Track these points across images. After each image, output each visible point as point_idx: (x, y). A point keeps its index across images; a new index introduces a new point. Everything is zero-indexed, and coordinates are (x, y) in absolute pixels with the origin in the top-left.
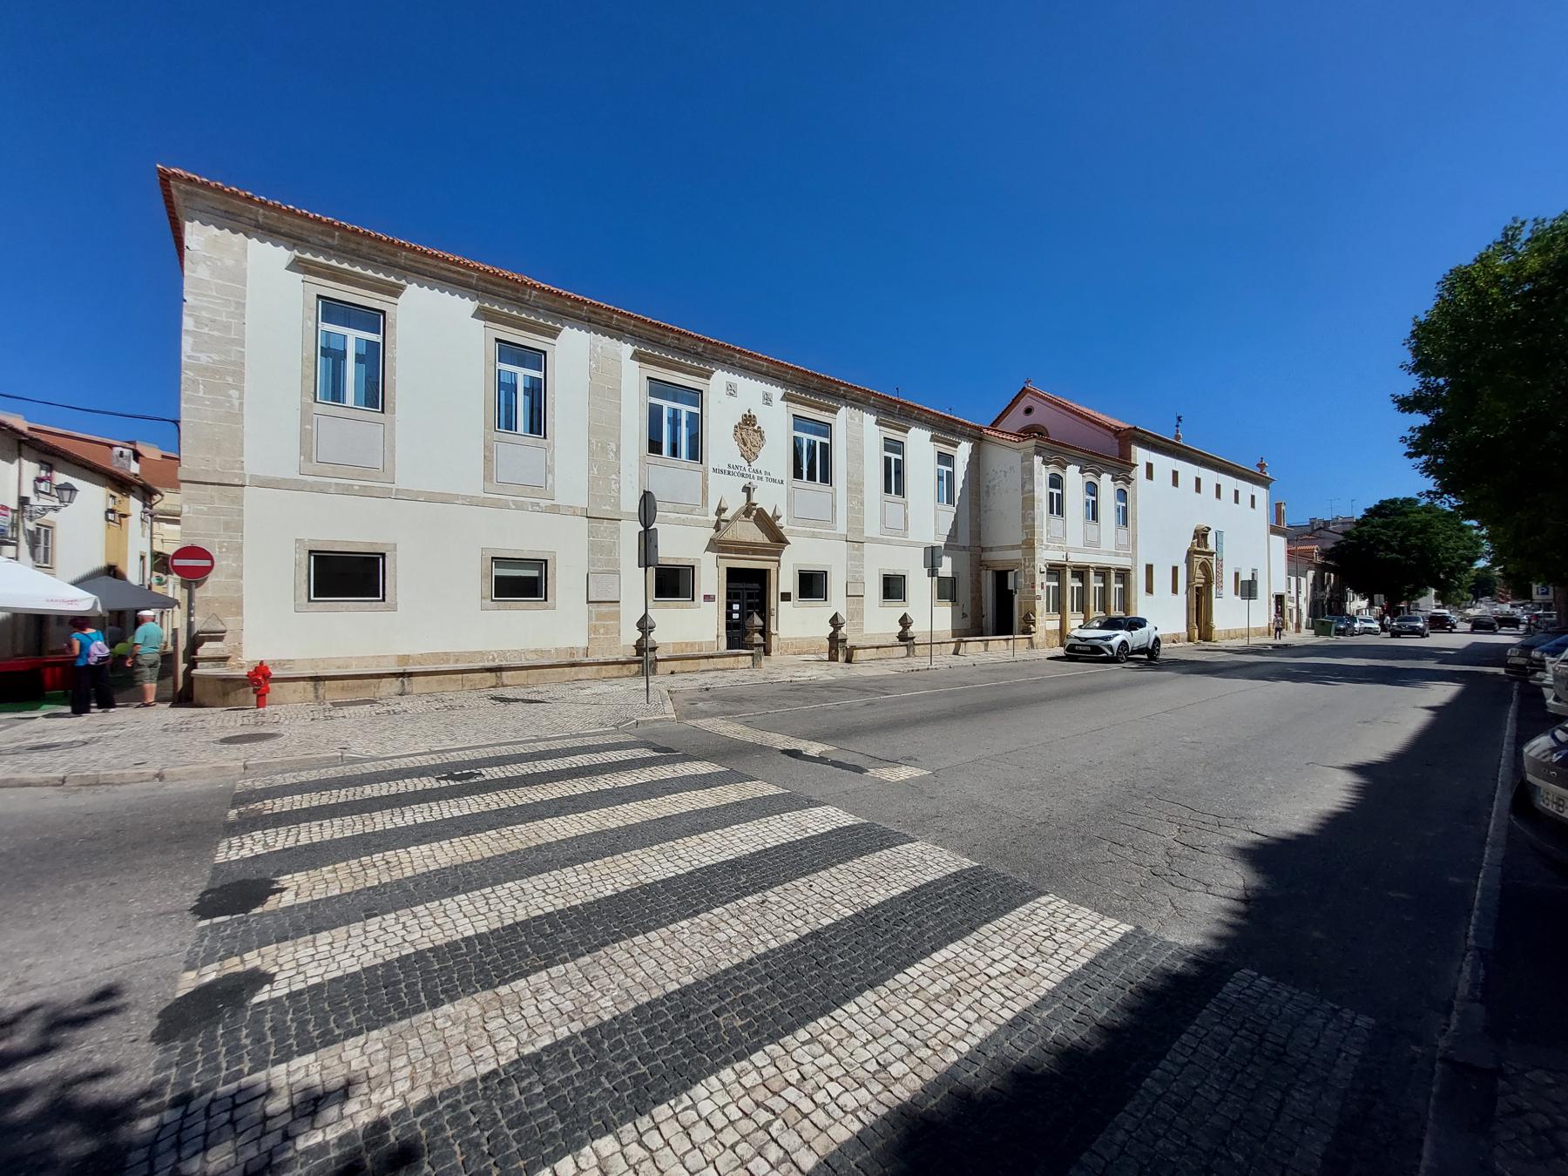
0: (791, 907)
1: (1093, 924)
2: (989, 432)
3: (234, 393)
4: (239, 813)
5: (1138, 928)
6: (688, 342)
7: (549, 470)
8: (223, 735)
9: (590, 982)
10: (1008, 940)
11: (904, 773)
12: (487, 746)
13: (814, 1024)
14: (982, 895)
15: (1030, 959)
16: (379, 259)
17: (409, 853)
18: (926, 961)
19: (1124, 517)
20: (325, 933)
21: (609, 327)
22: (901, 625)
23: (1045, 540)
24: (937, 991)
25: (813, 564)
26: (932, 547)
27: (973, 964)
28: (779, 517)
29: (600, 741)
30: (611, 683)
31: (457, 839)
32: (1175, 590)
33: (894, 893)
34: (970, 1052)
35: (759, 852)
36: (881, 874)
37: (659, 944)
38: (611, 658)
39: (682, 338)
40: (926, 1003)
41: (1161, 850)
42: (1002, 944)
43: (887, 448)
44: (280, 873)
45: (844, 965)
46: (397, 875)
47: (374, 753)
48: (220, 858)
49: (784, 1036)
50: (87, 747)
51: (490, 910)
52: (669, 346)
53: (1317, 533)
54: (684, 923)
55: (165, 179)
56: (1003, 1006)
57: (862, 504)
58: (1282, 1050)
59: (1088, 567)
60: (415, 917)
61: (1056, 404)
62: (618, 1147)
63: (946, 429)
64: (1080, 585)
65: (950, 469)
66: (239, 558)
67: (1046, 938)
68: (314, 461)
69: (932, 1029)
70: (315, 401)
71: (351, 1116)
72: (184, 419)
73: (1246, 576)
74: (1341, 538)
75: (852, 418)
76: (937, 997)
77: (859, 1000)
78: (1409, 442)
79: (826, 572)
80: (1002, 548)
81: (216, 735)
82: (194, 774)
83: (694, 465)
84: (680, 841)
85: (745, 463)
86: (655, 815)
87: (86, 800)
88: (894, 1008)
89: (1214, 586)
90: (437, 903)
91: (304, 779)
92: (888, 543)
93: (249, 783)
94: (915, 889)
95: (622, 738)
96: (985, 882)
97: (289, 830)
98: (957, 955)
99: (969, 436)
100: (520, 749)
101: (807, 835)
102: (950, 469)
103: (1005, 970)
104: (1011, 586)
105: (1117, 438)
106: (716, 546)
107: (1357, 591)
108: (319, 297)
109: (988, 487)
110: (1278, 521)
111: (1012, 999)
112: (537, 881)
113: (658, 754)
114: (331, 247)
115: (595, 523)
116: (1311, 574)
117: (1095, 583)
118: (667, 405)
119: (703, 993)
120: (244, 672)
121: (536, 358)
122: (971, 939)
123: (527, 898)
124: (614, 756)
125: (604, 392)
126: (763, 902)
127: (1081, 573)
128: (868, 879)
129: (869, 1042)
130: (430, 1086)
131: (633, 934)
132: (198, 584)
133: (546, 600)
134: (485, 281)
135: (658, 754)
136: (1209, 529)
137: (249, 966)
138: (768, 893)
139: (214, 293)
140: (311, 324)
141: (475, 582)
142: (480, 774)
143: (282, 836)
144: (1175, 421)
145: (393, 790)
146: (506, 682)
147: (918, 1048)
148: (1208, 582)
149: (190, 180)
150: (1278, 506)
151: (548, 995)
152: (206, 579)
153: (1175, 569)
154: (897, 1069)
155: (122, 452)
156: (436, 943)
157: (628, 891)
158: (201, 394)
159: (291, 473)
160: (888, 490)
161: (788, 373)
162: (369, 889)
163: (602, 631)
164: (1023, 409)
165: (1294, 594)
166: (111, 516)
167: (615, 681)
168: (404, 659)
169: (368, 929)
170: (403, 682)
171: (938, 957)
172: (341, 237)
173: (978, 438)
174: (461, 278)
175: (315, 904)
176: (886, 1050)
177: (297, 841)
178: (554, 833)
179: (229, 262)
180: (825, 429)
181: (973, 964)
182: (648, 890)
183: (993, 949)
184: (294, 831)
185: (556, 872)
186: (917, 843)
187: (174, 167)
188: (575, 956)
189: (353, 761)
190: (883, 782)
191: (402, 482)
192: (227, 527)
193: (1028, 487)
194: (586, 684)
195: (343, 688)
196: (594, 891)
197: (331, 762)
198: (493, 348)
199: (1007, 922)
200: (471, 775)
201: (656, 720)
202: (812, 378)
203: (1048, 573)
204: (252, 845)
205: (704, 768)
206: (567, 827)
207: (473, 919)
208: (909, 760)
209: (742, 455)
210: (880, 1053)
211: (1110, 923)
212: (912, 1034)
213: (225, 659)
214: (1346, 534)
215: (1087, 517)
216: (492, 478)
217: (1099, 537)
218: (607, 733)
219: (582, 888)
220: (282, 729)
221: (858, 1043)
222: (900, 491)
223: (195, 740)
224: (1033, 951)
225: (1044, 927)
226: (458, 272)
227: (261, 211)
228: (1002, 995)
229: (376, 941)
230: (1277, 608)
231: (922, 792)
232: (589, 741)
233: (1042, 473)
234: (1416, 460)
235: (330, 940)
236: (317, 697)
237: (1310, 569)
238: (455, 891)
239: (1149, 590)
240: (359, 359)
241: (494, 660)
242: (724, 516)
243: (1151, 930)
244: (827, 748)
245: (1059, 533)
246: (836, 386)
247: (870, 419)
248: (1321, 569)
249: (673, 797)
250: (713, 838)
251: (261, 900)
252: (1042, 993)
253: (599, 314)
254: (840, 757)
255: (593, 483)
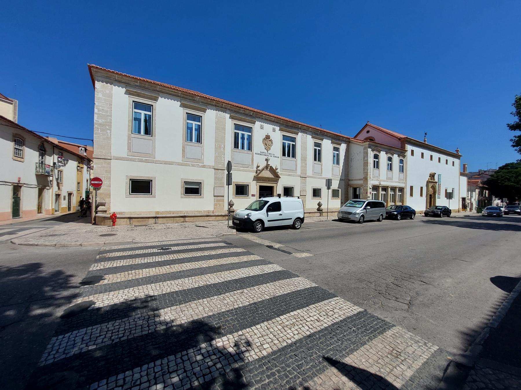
0: (250, 295)
1: (349, 307)
2: (352, 140)
3: (109, 131)
4: (100, 257)
5: (366, 310)
6: (247, 112)
7: (203, 154)
8: (102, 234)
9: (182, 312)
10: (318, 310)
11: (304, 255)
12: (175, 240)
13: (245, 330)
14: (315, 296)
15: (323, 317)
16: (151, 89)
17: (143, 271)
18: (288, 315)
19: (402, 169)
20: (113, 292)
21: (222, 108)
22: (318, 205)
23: (372, 177)
24: (287, 324)
25: (289, 184)
26: (329, 179)
27: (303, 317)
28: (277, 169)
29: (210, 240)
30: (219, 222)
31: (158, 268)
32: (421, 195)
33: (285, 293)
34: (291, 343)
35: (247, 277)
36: (283, 286)
37: (206, 302)
38: (220, 214)
39: (245, 110)
40: (283, 327)
41: (385, 285)
42: (315, 312)
43: (315, 146)
44: (105, 275)
45: (261, 313)
46: (137, 277)
47: (142, 241)
48: (91, 269)
49: (234, 333)
50: (64, 236)
51: (160, 289)
52: (241, 113)
53: (481, 175)
54: (216, 297)
55: (90, 68)
56: (308, 330)
57: (306, 165)
58: (399, 353)
59: (388, 187)
60: (138, 289)
61: (378, 129)
62: (175, 359)
63: (336, 139)
64: (393, 193)
65: (338, 153)
66: (110, 181)
67: (331, 311)
68: (132, 152)
69: (282, 335)
70: (132, 133)
71: (105, 342)
72: (94, 140)
73: (450, 191)
74: (490, 177)
75: (303, 135)
76: (287, 326)
77: (262, 324)
78: (513, 141)
79: (293, 187)
80: (356, 180)
81: (99, 234)
82: (90, 245)
83: (249, 152)
84: (223, 272)
85: (266, 151)
86: (219, 264)
87: (60, 251)
88: (272, 328)
89: (437, 194)
90: (146, 286)
91: (120, 248)
92: (315, 178)
93: (105, 248)
94: (293, 292)
95: (217, 239)
96: (318, 291)
97: (111, 262)
98: (299, 313)
99: (345, 141)
100: (185, 242)
101: (264, 273)
102: (338, 153)
103: (313, 319)
104: (358, 193)
105: (400, 141)
106: (257, 179)
107: (496, 197)
108: (133, 101)
109: (352, 158)
110: (464, 171)
111: (311, 329)
112: (176, 282)
113: (226, 245)
114: (137, 86)
115: (217, 171)
116: (477, 191)
117: (390, 193)
118: (240, 132)
119: (214, 318)
120: (109, 216)
121: (198, 118)
122: (305, 309)
123: (172, 286)
124: (212, 245)
125: (220, 128)
126: (242, 292)
127: (385, 189)
128: (278, 288)
129: (260, 337)
130: (128, 336)
131: (199, 299)
132: (99, 189)
133: (201, 195)
134: (183, 95)
135: (226, 245)
136: (435, 174)
137: (90, 300)
138: (245, 290)
139: (103, 102)
140: (131, 110)
141: (179, 189)
142: (171, 249)
143: (109, 264)
144: (424, 135)
145: (144, 252)
146: (187, 221)
147: (275, 340)
148: (434, 193)
149: (97, 68)
150: (464, 165)
151: (169, 315)
152: (101, 187)
153: (422, 188)
154: (265, 346)
155: (82, 149)
156: (142, 297)
157: (202, 286)
158: (99, 132)
159: (311, 175)
160: (315, 160)
161: (281, 121)
162: (128, 280)
163: (218, 205)
164: (366, 131)
165: (469, 198)
166: (78, 168)
167: (221, 221)
168: (157, 213)
169: (124, 292)
170: (156, 220)
171: (292, 313)
172: (140, 83)
173: (348, 142)
174: (176, 94)
175: (112, 284)
176: (265, 340)
177: (113, 265)
178: (186, 268)
179: (108, 92)
180: (293, 140)
181: (303, 317)
182: (208, 286)
183: (311, 313)
184: (113, 263)
185: (183, 279)
186: (299, 278)
187: (93, 64)
188: (180, 304)
189: (135, 243)
190: (296, 257)
191: (157, 158)
192: (106, 171)
193: (366, 159)
194: (211, 222)
195: (138, 221)
196: (192, 285)
197: (128, 243)
198: (185, 116)
199: (320, 304)
200: (168, 249)
201: (229, 234)
202: (289, 123)
203: (373, 189)
204: (101, 266)
205: (239, 250)
206: (191, 266)
207: (154, 291)
208: (308, 251)
209: (265, 149)
210: (262, 341)
211: (356, 307)
212: (275, 336)
213: (105, 211)
214: (492, 176)
215: (388, 169)
216: (185, 157)
217: (392, 176)
218: (213, 238)
219: (189, 284)
220: (118, 233)
221: (257, 337)
222: (320, 160)
223: (93, 235)
224: (325, 314)
225: (332, 307)
226: (175, 92)
227: (117, 76)
228: (309, 327)
229: (126, 295)
230: (463, 203)
231: (308, 261)
232: (207, 240)
233: (371, 154)
234: (515, 148)
235: (113, 294)
236: (130, 223)
237: (477, 188)
238: (152, 282)
239: (411, 195)
240: (288, 146)
241: (184, 214)
242: (258, 169)
243: (369, 311)
244: (282, 245)
245: (377, 175)
246: (298, 125)
247: (309, 137)
248: (482, 189)
249: (226, 259)
250: (234, 272)
251: (99, 282)
252: (322, 327)
253: (219, 104)
254: (285, 249)
255: (216, 158)
